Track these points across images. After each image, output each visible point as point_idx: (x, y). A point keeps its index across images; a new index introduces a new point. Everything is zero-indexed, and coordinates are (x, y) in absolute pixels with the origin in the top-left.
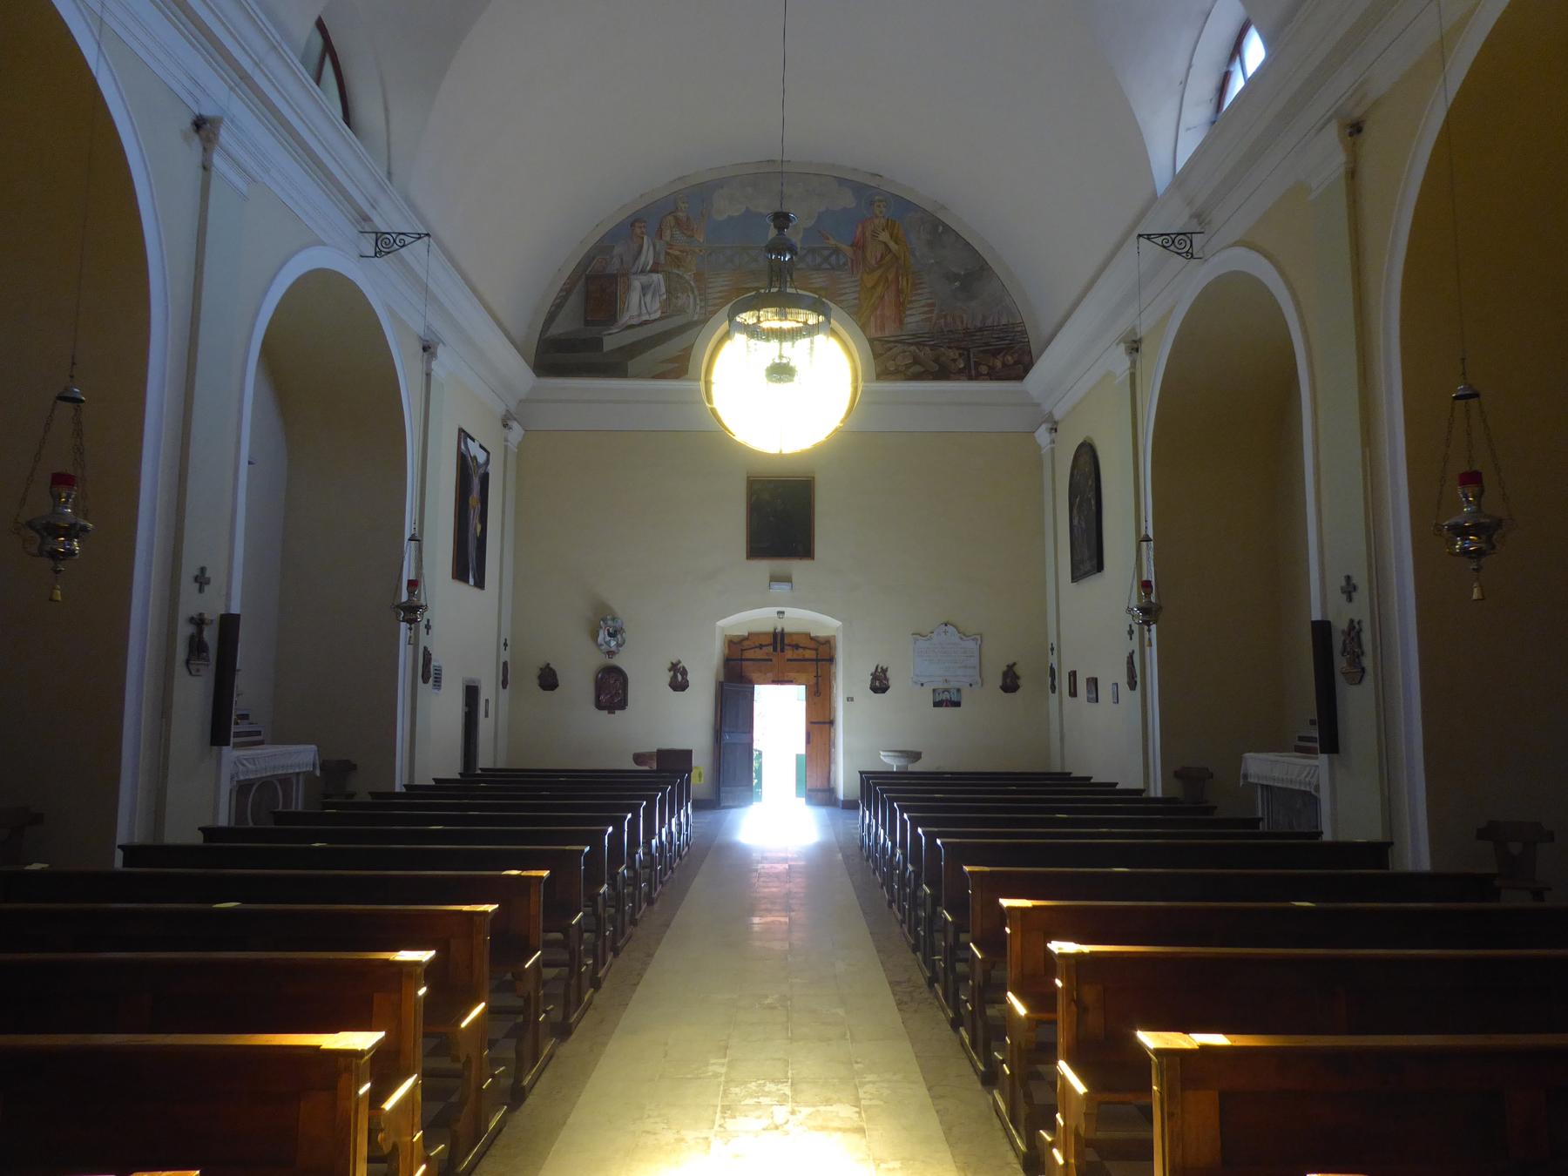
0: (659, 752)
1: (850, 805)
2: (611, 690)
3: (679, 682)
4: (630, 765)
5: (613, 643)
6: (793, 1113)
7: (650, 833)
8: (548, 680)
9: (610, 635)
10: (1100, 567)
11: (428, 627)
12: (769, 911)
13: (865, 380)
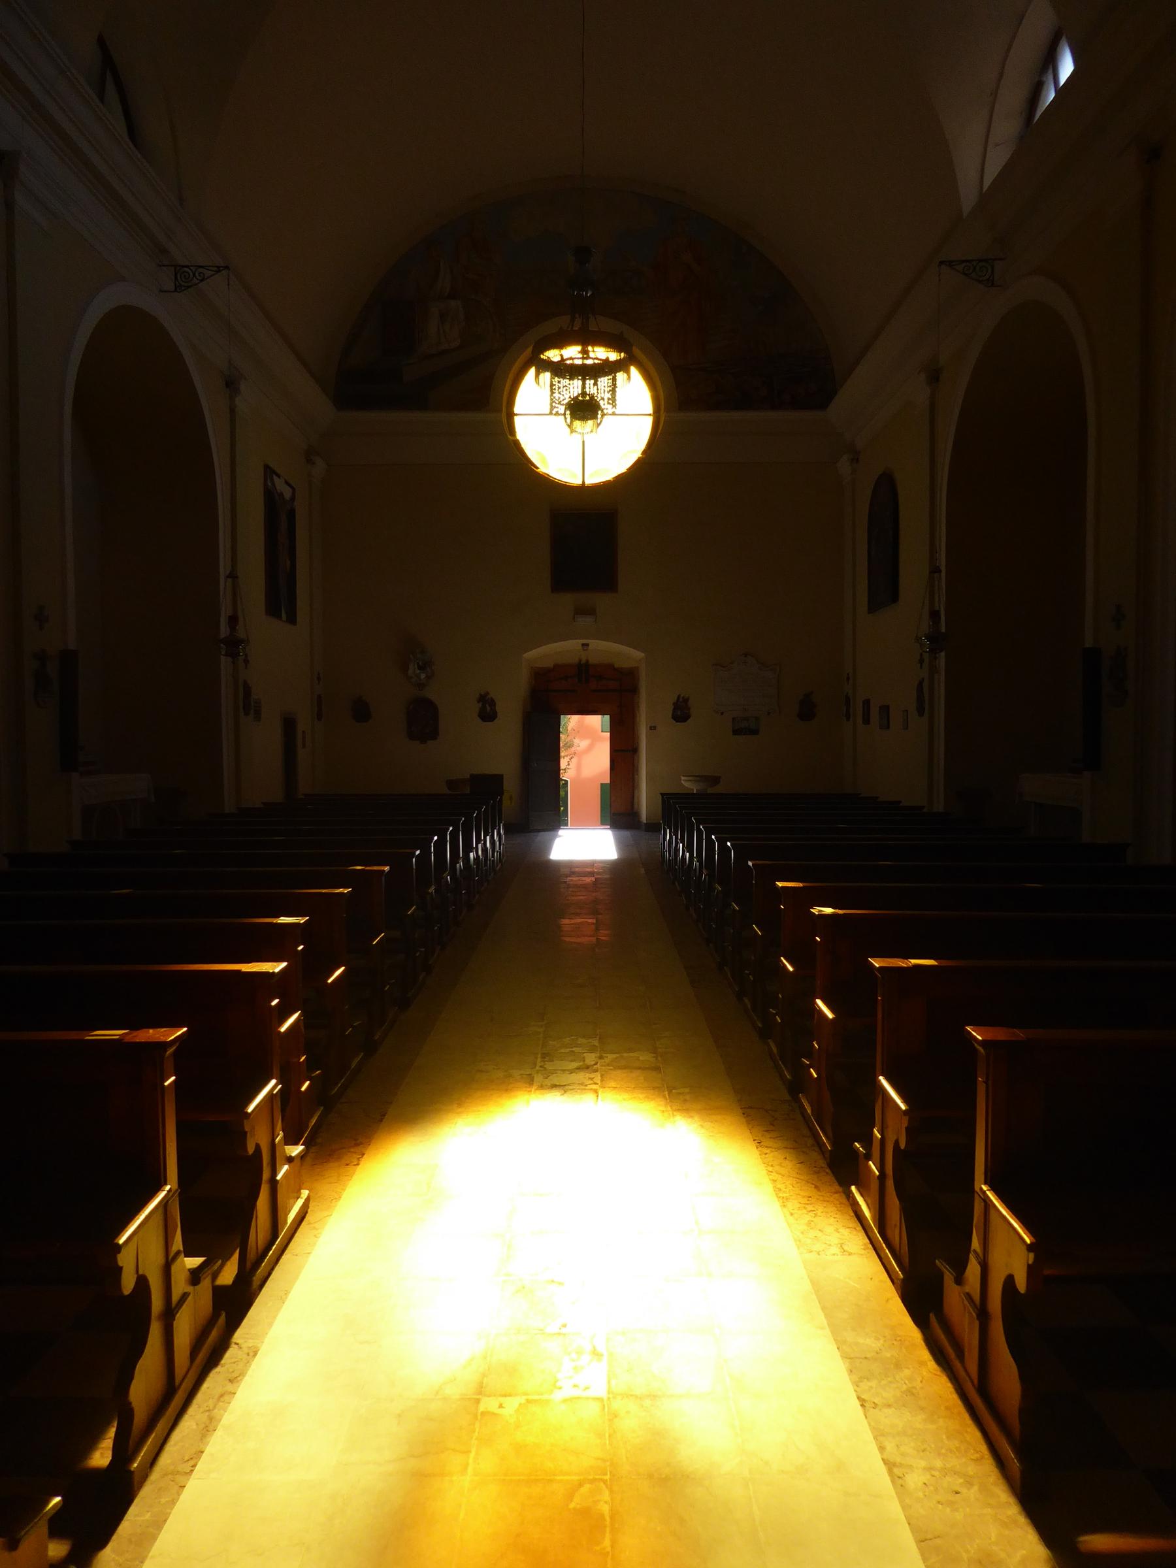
0: (472, 776)
1: (653, 828)
2: (423, 720)
3: (488, 712)
4: (446, 791)
5: (423, 676)
6: (601, 1058)
7: (468, 848)
8: (361, 711)
9: (420, 668)
10: (894, 598)
11: (246, 661)
12: (578, 914)
13: (667, 410)
